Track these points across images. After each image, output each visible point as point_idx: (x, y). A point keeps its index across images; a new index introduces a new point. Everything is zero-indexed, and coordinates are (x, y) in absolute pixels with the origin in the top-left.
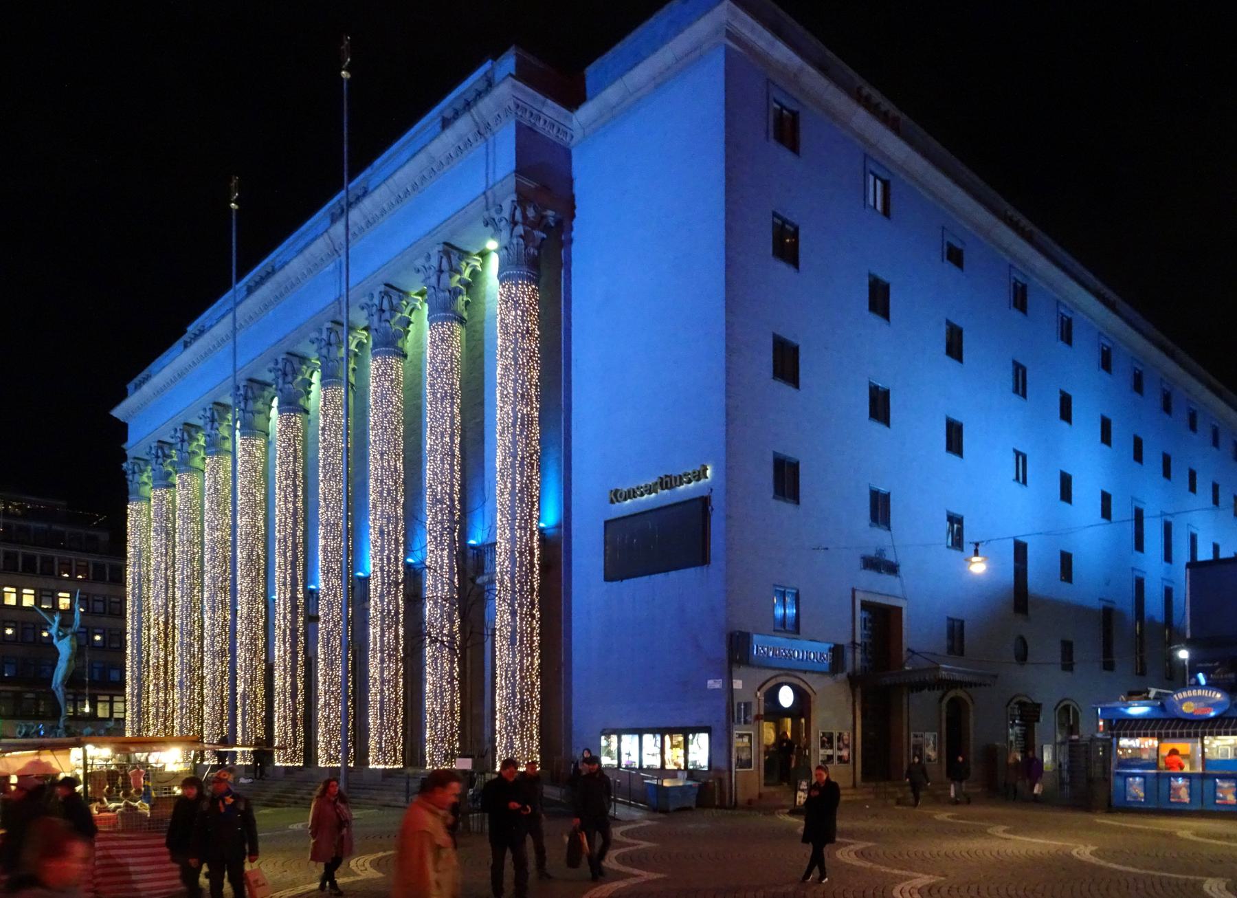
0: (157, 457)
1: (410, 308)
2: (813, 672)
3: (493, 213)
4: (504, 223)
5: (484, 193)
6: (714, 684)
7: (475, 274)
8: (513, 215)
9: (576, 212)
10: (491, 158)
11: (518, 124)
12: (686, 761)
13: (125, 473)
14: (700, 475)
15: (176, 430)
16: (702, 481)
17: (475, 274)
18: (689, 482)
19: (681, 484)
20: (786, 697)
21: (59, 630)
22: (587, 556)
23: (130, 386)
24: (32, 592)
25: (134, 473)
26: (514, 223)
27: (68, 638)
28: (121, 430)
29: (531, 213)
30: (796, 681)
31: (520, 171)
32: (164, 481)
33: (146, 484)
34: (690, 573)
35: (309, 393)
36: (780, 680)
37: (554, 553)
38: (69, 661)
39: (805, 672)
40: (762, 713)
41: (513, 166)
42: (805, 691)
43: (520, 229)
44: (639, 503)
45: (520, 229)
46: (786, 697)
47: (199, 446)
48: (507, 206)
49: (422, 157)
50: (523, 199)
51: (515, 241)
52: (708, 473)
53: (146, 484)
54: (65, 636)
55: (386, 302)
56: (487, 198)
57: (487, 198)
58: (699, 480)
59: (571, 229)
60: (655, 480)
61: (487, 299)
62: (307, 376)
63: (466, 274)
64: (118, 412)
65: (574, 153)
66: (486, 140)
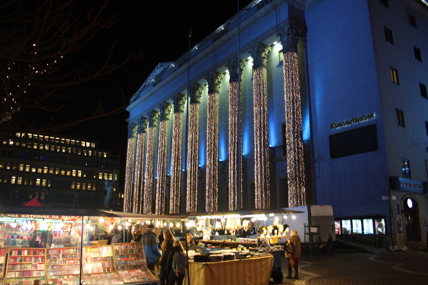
0: (141, 122)
1: (243, 65)
2: (418, 193)
3: (281, 31)
4: (285, 35)
5: (276, 26)
6: (384, 198)
7: (269, 52)
8: (288, 32)
9: (308, 30)
10: (278, 16)
11: (289, 5)
12: (352, 230)
13: (128, 129)
14: (370, 116)
15: (149, 113)
16: (371, 119)
17: (269, 52)
18: (366, 119)
19: (363, 120)
20: (410, 204)
21: (108, 183)
22: (323, 150)
23: (132, 99)
24: (29, 166)
25: (131, 128)
26: (289, 34)
27: (110, 186)
28: (127, 114)
29: (294, 31)
30: (412, 197)
31: (290, 18)
32: (142, 131)
33: (135, 132)
34: (369, 154)
35: (201, 96)
36: (408, 196)
37: (308, 149)
38: (110, 195)
39: (415, 193)
40: (403, 210)
41: (287, 17)
42: (416, 202)
43: (291, 36)
44: (344, 128)
45: (291, 36)
46: (410, 204)
47: (156, 118)
48: (286, 29)
49: (252, 18)
50: (292, 27)
51: (289, 40)
52: (374, 115)
53: (135, 132)
54: (110, 185)
55: (235, 64)
56: (277, 28)
57: (277, 28)
58: (371, 118)
59: (306, 36)
60: (351, 120)
61: (273, 60)
62: (200, 91)
63: (267, 53)
64: (128, 109)
65: (305, 12)
66: (276, 10)
